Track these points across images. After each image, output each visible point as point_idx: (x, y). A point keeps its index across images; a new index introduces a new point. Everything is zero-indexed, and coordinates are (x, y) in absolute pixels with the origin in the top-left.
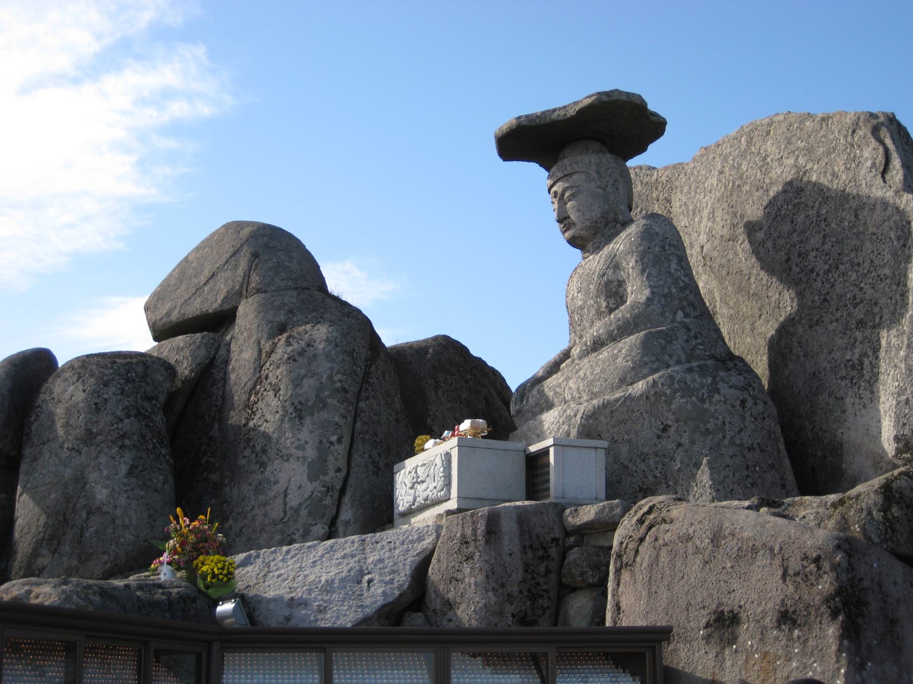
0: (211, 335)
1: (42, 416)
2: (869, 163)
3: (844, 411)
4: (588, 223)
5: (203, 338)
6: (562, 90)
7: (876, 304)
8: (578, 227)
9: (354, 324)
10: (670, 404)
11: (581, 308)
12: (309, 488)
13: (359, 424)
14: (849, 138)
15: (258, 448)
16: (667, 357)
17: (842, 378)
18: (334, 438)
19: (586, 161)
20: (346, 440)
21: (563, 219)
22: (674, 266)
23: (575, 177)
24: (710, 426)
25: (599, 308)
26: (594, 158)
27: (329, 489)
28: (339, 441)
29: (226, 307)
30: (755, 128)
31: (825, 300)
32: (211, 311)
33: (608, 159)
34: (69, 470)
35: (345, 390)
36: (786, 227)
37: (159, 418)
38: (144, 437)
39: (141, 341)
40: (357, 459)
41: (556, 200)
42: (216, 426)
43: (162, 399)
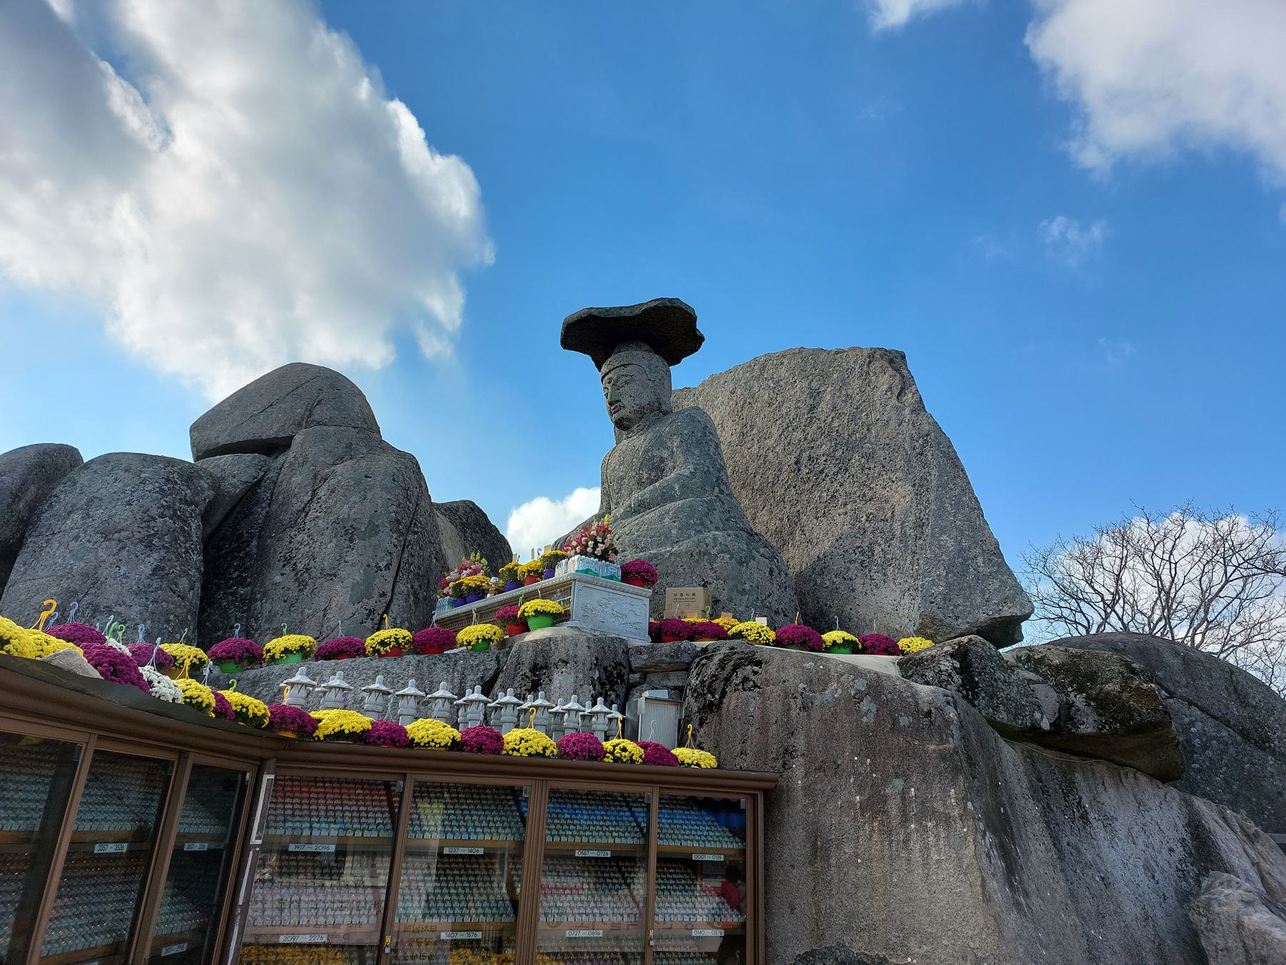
0: (263, 457)
1: (57, 506)
2: (885, 387)
3: (853, 590)
4: (636, 408)
5: (253, 458)
6: (627, 292)
7: (887, 502)
8: (627, 410)
9: (408, 472)
10: (281, 874)
11: (622, 478)
12: (352, 609)
13: (406, 555)
14: (865, 368)
15: (300, 566)
16: (708, 523)
17: (851, 562)
18: (383, 564)
19: (638, 359)
20: (395, 564)
21: (614, 403)
22: (712, 450)
23: (630, 368)
24: (747, 587)
25: (640, 479)
26: (646, 355)
27: (371, 612)
28: (387, 567)
29: (282, 435)
30: (769, 357)
31: (833, 496)
32: (264, 437)
33: (657, 360)
34: (82, 564)
35: (398, 522)
36: (798, 435)
37: (195, 524)
38: (176, 539)
39: (186, 454)
40: (401, 587)
41: (609, 386)
42: (254, 543)
43: (202, 507)
